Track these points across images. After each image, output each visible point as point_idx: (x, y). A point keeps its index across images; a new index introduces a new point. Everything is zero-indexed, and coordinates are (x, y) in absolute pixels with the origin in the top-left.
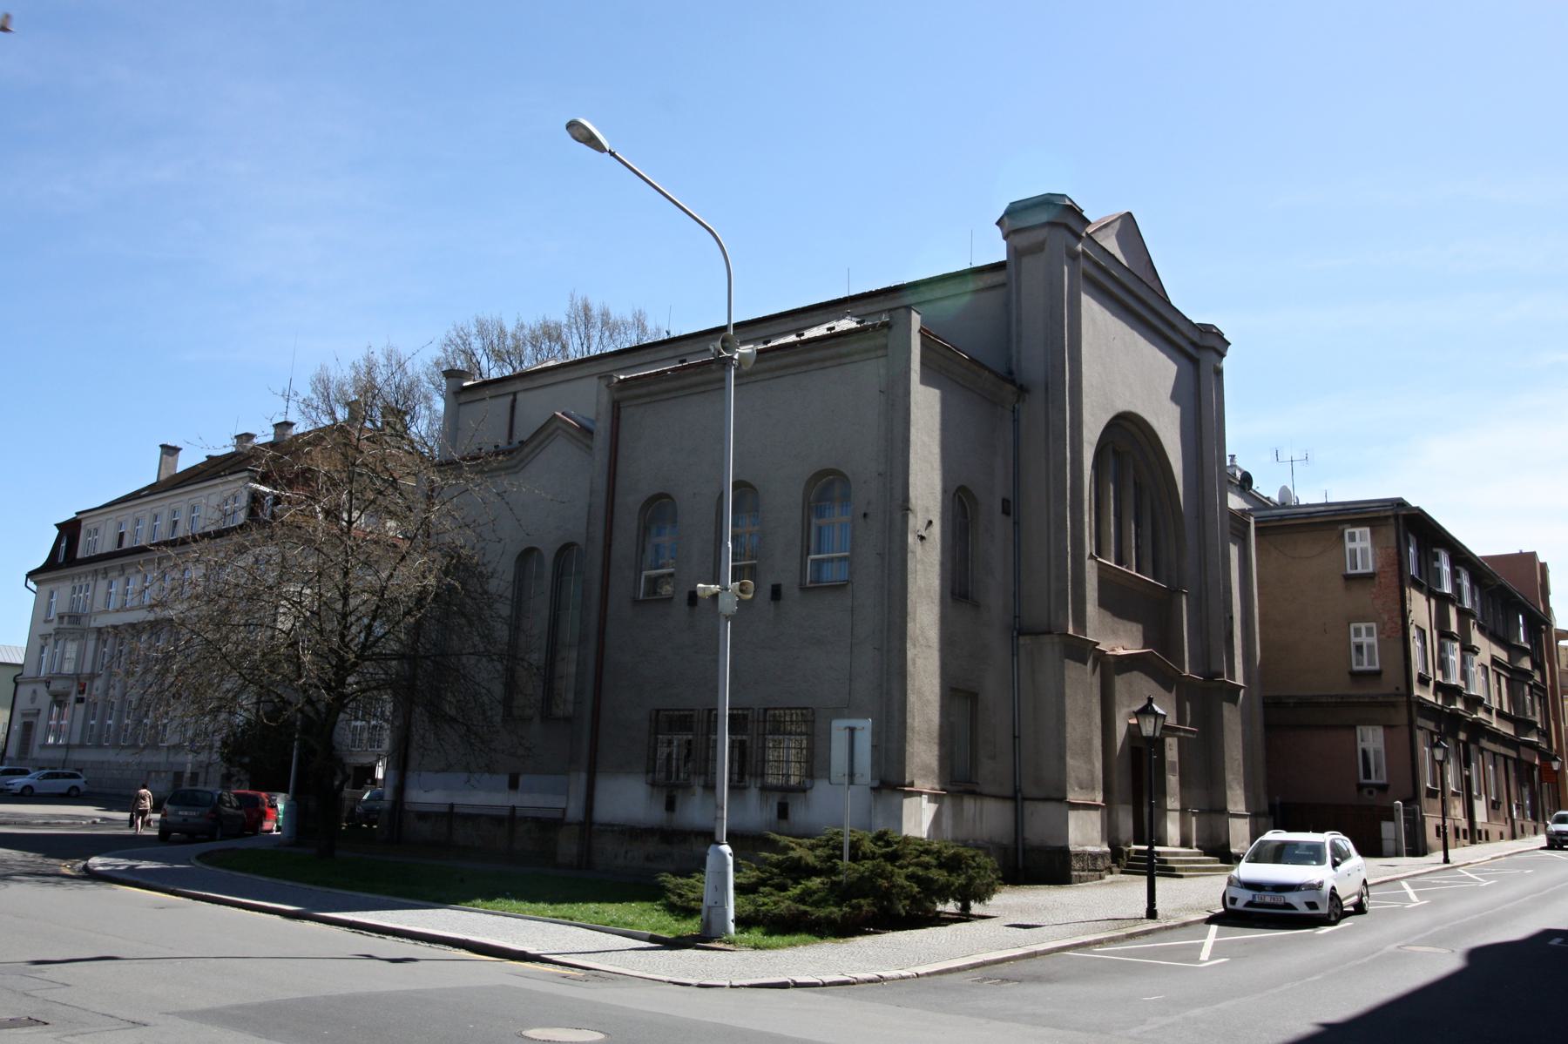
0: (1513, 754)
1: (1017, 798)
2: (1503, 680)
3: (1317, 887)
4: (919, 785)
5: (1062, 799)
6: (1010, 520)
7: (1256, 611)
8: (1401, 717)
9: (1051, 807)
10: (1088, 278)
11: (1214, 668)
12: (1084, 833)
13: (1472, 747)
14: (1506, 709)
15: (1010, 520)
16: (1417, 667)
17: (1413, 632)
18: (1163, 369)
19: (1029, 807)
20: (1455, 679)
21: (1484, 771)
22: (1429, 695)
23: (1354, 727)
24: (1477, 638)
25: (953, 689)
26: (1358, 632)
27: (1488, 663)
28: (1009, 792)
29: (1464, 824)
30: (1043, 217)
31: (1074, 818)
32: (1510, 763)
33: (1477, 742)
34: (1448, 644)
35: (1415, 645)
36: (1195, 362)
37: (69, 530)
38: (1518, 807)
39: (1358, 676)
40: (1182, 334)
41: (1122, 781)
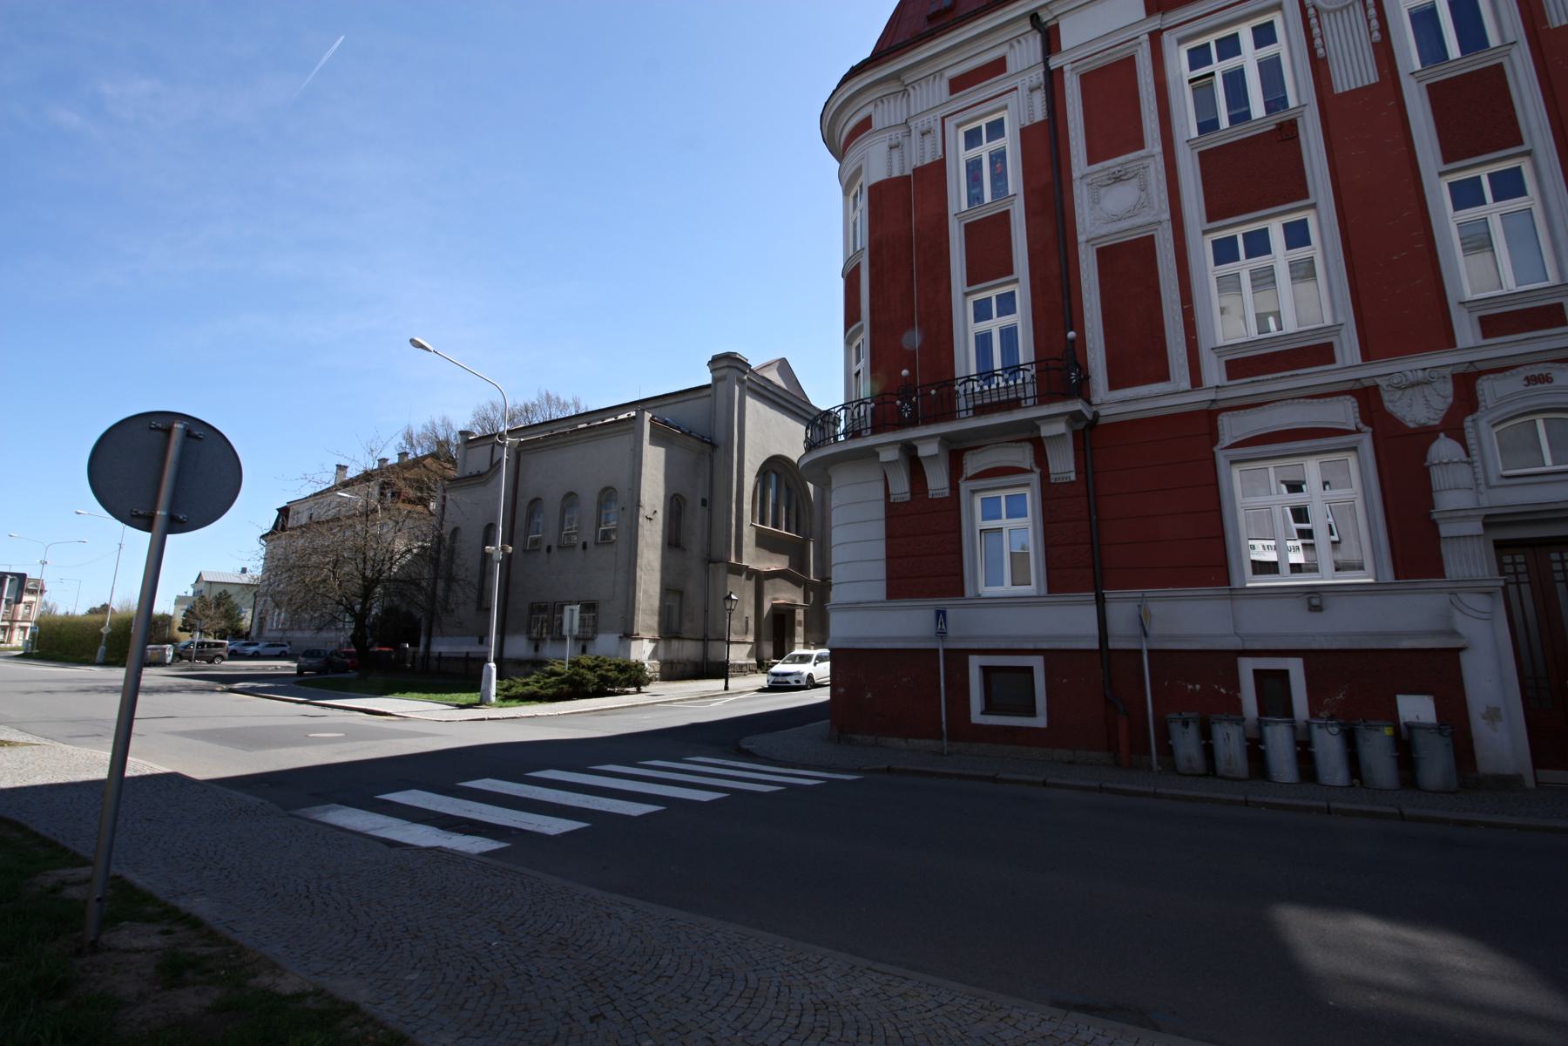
1: (705, 640)
3: (799, 674)
4: (642, 634)
12: (738, 655)
28: (700, 636)
37: (284, 512)
41: (767, 630)
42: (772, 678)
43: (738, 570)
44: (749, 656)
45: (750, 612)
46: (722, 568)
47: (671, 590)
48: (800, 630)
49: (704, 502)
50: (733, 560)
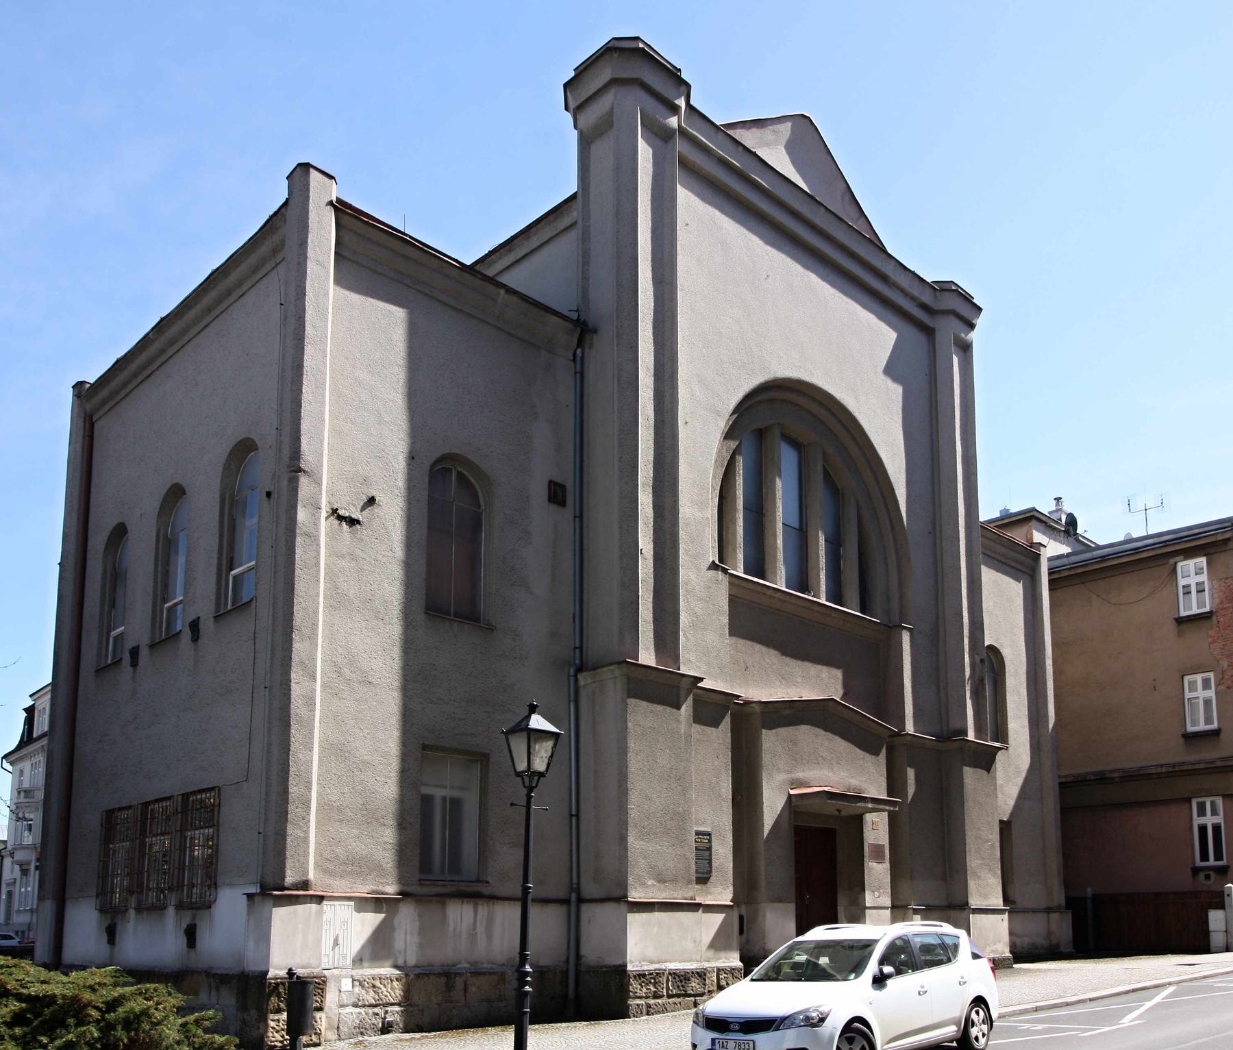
5: (619, 898)
6: (569, 512)
7: (1049, 662)
9: (610, 908)
10: (684, 164)
18: (878, 336)
19: (587, 911)
23: (1189, 800)
25: (425, 747)
31: (636, 924)
36: (929, 332)
39: (1191, 738)
40: (906, 294)
41: (776, 868)
43: (667, 688)
44: (719, 943)
45: (717, 818)
48: (878, 872)
49: (556, 494)
50: (647, 657)
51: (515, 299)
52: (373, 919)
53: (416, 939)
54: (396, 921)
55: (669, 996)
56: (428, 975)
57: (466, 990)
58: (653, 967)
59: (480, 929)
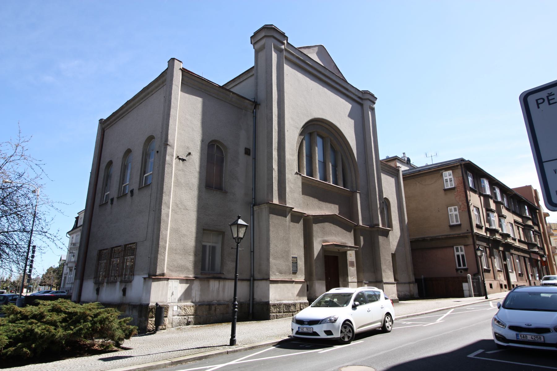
0: (528, 256)
2: (521, 229)
5: (267, 279)
6: (250, 158)
8: (470, 241)
9: (263, 283)
11: (375, 222)
12: (169, 293)
13: (507, 253)
14: (523, 239)
15: (250, 158)
16: (475, 222)
17: (472, 208)
19: (256, 282)
20: (495, 226)
21: (513, 262)
22: (483, 233)
23: (453, 247)
24: (504, 212)
26: (451, 210)
27: (513, 222)
29: (505, 283)
30: (263, 34)
31: (272, 287)
32: (527, 260)
33: (509, 251)
34: (491, 214)
35: (474, 213)
36: (361, 105)
38: (532, 275)
41: (319, 269)
42: (296, 327)
43: (282, 211)
44: (300, 294)
45: (299, 252)
46: (265, 209)
47: (210, 229)
49: (247, 152)
50: (276, 201)
51: (235, 95)
52: (185, 286)
53: (199, 293)
54: (193, 286)
55: (284, 312)
56: (203, 305)
57: (215, 310)
58: (278, 302)
59: (221, 289)
